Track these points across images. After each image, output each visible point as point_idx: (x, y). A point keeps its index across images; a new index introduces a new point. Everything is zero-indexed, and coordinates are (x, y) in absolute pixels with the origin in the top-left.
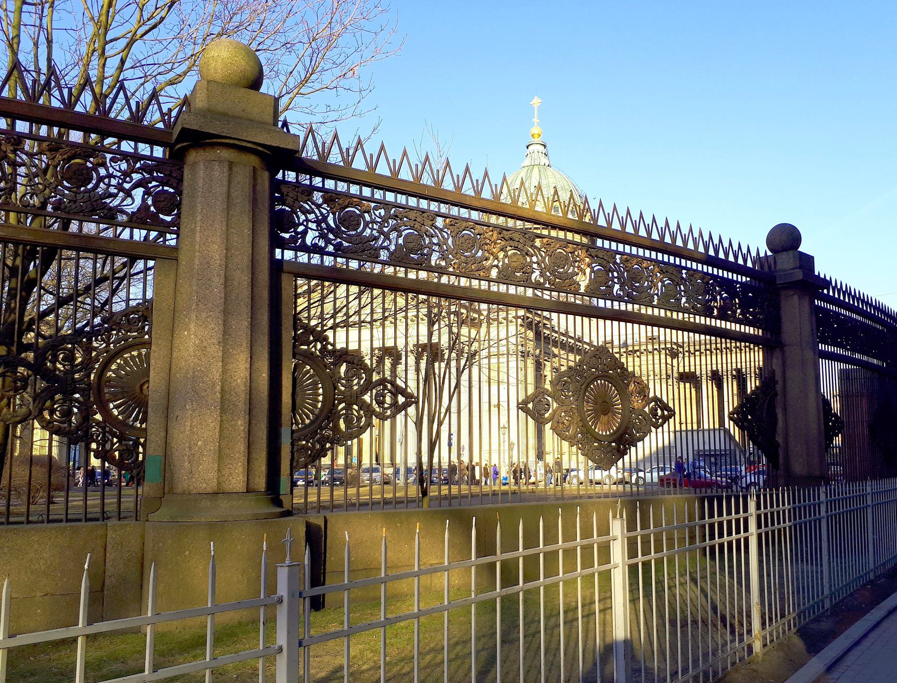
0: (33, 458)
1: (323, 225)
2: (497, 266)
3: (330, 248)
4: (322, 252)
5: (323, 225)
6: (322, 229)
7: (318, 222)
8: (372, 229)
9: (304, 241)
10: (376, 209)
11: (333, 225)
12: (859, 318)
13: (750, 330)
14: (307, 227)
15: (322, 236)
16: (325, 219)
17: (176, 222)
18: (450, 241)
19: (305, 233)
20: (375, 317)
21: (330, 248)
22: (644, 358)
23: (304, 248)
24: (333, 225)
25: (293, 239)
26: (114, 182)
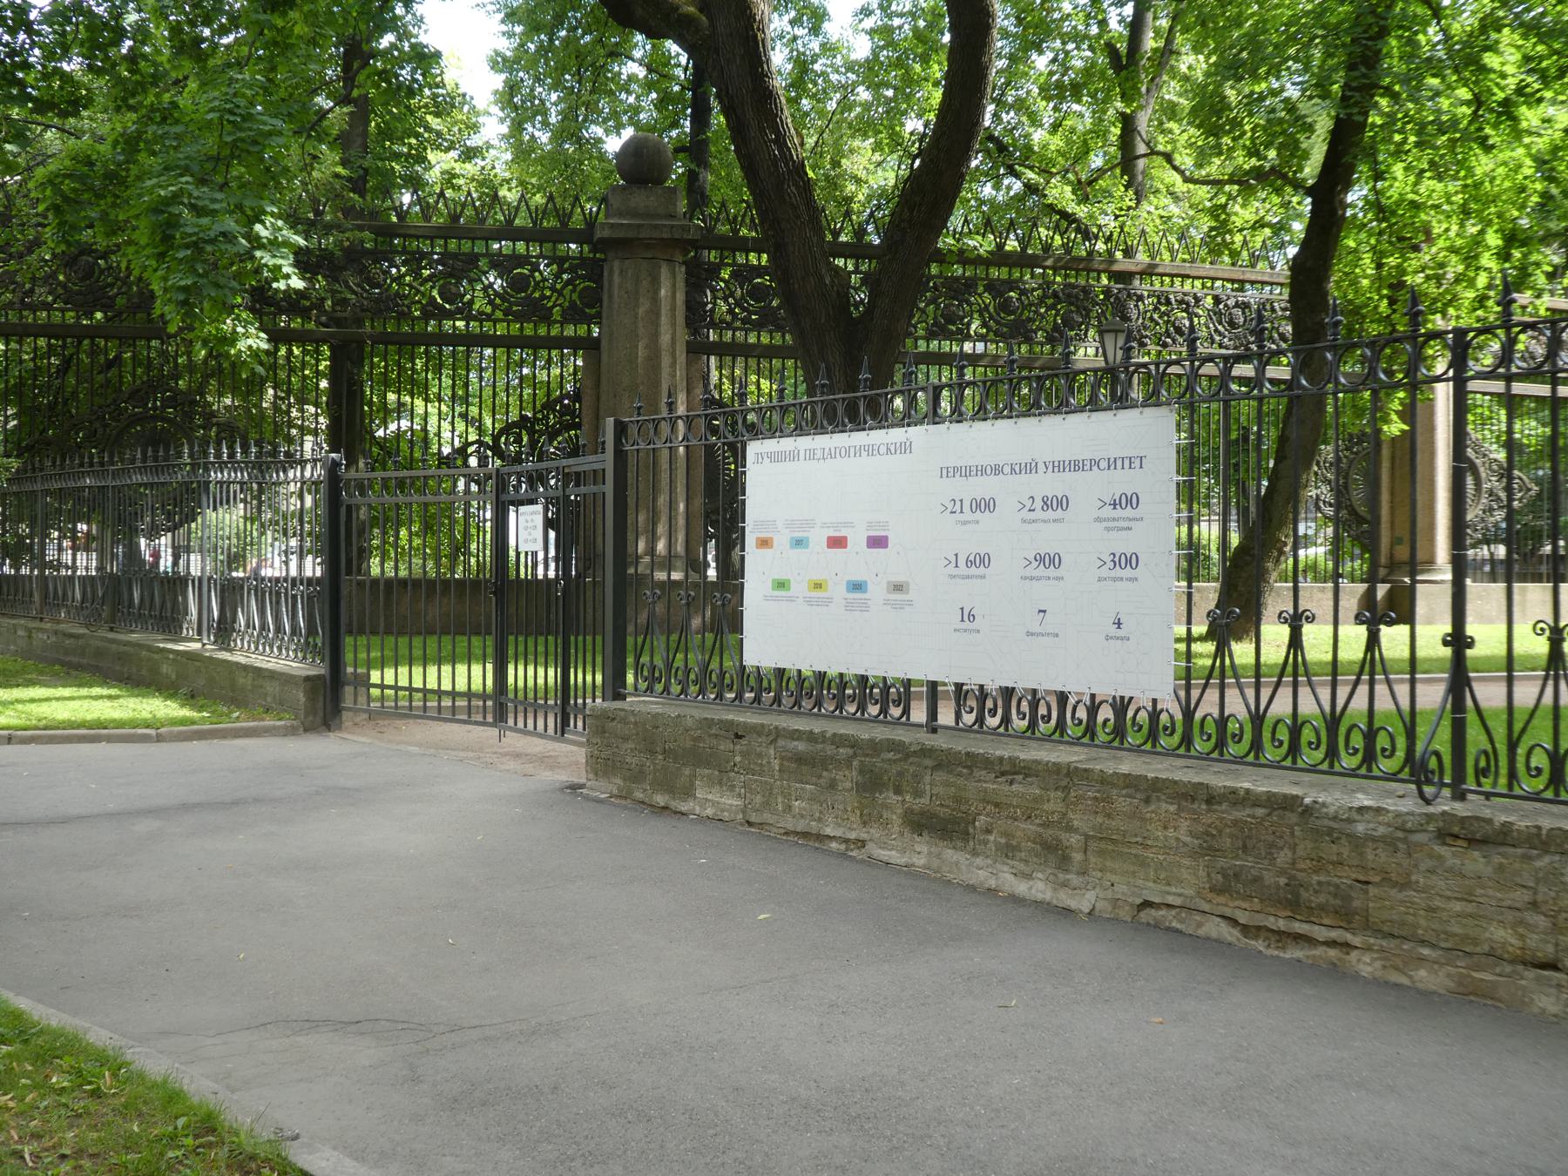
4: (489, 317)
17: (599, 315)
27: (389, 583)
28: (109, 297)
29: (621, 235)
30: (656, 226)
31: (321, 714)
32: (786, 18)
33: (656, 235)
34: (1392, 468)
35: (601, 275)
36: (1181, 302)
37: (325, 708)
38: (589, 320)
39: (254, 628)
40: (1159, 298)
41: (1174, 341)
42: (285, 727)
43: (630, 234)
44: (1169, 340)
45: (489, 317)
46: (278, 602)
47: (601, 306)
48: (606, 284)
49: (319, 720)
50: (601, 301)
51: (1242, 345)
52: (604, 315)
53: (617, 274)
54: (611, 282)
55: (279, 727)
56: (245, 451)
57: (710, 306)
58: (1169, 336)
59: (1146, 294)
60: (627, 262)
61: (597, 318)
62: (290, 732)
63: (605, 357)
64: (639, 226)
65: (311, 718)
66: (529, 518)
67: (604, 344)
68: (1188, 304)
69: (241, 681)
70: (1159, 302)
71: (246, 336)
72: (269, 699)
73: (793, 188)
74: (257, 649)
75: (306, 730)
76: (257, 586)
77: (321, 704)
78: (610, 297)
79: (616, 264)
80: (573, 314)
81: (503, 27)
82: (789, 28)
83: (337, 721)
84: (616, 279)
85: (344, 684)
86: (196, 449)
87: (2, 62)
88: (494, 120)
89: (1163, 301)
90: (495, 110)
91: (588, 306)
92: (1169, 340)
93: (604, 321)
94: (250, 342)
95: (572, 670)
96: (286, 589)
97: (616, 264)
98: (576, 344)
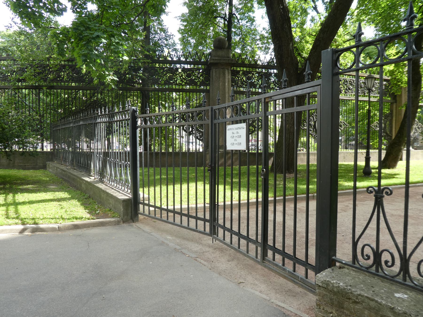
0: (238, 189)
1: (182, 78)
2: (199, 81)
3: (183, 84)
4: (181, 84)
5: (182, 78)
6: (181, 79)
7: (180, 77)
8: (195, 77)
9: (176, 82)
10: (256, 74)
11: (245, 80)
12: (216, 202)
13: (277, 139)
14: (177, 79)
15: (181, 81)
16: (243, 78)
17: (209, 84)
18: (244, 78)
19: (176, 81)
20: (90, 109)
21: (183, 84)
22: (177, 206)
23: (176, 84)
24: (245, 80)
25: (174, 83)
26: (256, 79)
27: (157, 154)
28: (83, 79)
29: (216, 62)
30: (225, 60)
31: (130, 214)
32: (245, 21)
33: (225, 62)
34: (396, 123)
35: (210, 73)
36: (350, 81)
37: (131, 212)
38: (207, 85)
39: (108, 175)
40: (345, 80)
41: (348, 91)
42: (115, 221)
43: (218, 62)
44: (347, 91)
45: (181, 84)
46: (115, 167)
47: (210, 82)
48: (211, 75)
49: (129, 217)
50: (210, 80)
51: (363, 92)
52: (211, 83)
53: (214, 73)
54: (212, 75)
55: (112, 221)
56: (105, 111)
57: (237, 82)
58: (347, 90)
59: (342, 79)
60: (217, 69)
61: (209, 85)
62: (117, 223)
63: (211, 94)
64: (220, 59)
65: (126, 217)
66: (235, 131)
67: (211, 91)
68: (351, 82)
69: (103, 196)
70: (345, 81)
71: (109, 75)
72: (111, 205)
73: (286, 26)
74: (109, 183)
75: (124, 222)
76: (109, 160)
77: (130, 211)
78: (212, 79)
79: (214, 70)
80: (203, 83)
81: (181, 23)
82: (246, 24)
83: (137, 218)
84: (214, 74)
85: (139, 204)
86: (92, 112)
87: (41, 1)
88: (179, 45)
89: (346, 81)
90: (180, 42)
91: (207, 81)
92: (347, 91)
93: (211, 85)
94: (110, 77)
95: (216, 186)
96: (118, 162)
97: (214, 70)
98: (203, 91)
